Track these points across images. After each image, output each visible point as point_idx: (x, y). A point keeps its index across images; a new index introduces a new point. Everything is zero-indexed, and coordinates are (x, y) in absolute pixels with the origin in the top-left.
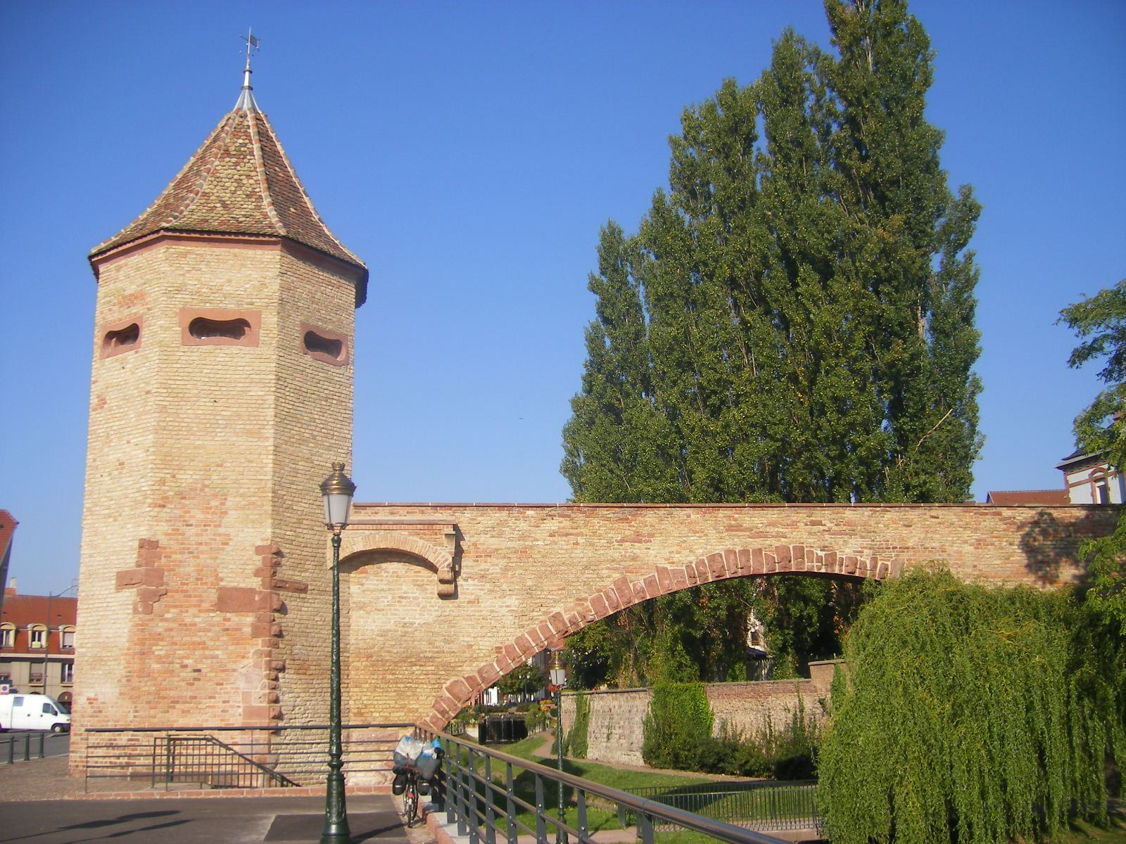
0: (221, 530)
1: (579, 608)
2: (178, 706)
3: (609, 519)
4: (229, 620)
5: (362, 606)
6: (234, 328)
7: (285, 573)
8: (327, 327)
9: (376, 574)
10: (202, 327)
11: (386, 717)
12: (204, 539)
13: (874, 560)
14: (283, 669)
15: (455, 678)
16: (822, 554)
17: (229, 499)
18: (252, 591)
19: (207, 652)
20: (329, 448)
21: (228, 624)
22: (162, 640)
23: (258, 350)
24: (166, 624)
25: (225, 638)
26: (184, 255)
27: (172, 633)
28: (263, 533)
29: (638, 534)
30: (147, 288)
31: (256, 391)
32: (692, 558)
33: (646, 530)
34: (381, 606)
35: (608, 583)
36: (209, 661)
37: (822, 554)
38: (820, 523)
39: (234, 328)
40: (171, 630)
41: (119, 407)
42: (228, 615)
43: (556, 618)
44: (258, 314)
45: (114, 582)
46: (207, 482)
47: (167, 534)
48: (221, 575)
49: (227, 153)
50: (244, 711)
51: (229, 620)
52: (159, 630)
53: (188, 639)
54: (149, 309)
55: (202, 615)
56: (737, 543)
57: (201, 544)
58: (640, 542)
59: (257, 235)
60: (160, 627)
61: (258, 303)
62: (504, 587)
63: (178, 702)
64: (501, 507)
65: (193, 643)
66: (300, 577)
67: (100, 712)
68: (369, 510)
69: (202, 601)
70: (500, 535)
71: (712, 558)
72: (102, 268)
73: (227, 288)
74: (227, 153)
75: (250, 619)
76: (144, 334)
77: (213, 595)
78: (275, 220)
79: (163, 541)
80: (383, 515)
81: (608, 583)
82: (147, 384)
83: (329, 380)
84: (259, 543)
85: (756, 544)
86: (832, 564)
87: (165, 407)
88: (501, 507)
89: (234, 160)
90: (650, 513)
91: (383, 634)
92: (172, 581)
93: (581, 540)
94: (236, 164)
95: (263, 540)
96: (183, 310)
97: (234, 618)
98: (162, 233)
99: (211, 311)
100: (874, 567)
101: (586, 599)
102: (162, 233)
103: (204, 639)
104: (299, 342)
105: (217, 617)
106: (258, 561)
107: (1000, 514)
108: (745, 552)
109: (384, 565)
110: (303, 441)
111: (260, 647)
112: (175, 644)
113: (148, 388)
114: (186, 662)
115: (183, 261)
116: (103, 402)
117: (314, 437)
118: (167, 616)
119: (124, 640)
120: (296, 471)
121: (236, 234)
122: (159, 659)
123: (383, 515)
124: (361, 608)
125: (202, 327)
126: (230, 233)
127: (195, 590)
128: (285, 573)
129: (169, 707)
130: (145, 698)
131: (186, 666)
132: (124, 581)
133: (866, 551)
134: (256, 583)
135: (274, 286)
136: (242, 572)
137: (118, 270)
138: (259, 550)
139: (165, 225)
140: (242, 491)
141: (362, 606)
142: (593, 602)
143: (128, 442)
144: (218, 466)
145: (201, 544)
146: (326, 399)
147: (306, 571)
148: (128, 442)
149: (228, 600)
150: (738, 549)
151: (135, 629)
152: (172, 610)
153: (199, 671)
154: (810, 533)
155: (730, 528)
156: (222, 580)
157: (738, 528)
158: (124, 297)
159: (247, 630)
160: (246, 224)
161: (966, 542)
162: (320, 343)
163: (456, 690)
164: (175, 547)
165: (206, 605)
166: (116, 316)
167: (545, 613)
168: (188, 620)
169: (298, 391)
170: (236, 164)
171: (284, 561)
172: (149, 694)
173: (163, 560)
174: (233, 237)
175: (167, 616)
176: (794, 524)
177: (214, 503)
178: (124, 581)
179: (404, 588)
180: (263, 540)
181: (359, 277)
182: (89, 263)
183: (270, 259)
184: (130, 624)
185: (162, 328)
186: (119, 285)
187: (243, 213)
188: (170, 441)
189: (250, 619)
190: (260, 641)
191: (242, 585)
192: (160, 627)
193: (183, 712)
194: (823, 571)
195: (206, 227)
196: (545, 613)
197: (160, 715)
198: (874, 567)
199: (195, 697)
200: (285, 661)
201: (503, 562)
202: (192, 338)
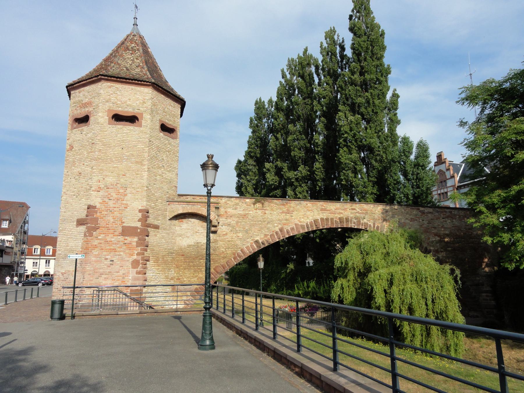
0: (125, 202)
1: (266, 238)
2: (103, 276)
3: (277, 204)
4: (126, 239)
5: (180, 235)
6: (132, 119)
7: (150, 221)
8: (170, 123)
9: (187, 223)
10: (118, 118)
11: (189, 281)
12: (117, 206)
13: (374, 224)
14: (148, 260)
15: (217, 265)
16: (355, 221)
17: (128, 189)
18: (137, 228)
19: (117, 253)
20: (169, 171)
21: (126, 241)
22: (97, 248)
23: (142, 129)
24: (98, 241)
25: (125, 247)
26: (110, 87)
27: (101, 245)
28: (142, 204)
29: (288, 210)
30: (93, 100)
31: (140, 146)
32: (308, 221)
33: (292, 209)
34: (188, 235)
35: (277, 229)
36: (117, 257)
37: (355, 221)
38: (354, 209)
39: (132, 119)
40: (101, 243)
41: (79, 150)
42: (126, 238)
43: (257, 242)
44: (142, 114)
45: (75, 223)
46: (118, 182)
47: (100, 203)
48: (123, 221)
49: (127, 49)
50: (132, 278)
51: (126, 239)
52: (95, 243)
53: (109, 247)
54: (94, 109)
55: (115, 237)
56: (324, 215)
57: (115, 207)
58: (289, 213)
59: (141, 81)
60: (96, 242)
61: (142, 109)
62: (237, 229)
63: (103, 274)
64: (227, 197)
65: (111, 249)
66: (156, 223)
67: (67, 279)
68: (184, 197)
69: (115, 231)
70: (236, 209)
71: (316, 221)
72: (72, 92)
73: (128, 102)
74: (127, 49)
75: (136, 239)
76: (92, 119)
77: (120, 229)
78: (150, 76)
79: (98, 205)
80: (190, 199)
81: (277, 229)
82: (93, 140)
83: (170, 144)
84: (140, 208)
85: (331, 216)
86: (359, 225)
87: (100, 150)
88: (227, 197)
89: (131, 52)
90: (293, 202)
91: (189, 246)
92: (102, 223)
93: (267, 212)
94: (131, 54)
95: (142, 206)
96: (109, 110)
97: (129, 239)
98: (100, 77)
99: (122, 111)
100: (374, 227)
101: (268, 235)
102: (100, 77)
103: (115, 248)
104: (158, 127)
105: (121, 238)
106: (140, 215)
107: (419, 209)
108: (327, 219)
109: (190, 219)
110: (159, 168)
111: (139, 251)
112: (103, 249)
113: (93, 142)
114: (107, 257)
115: (110, 89)
116: (72, 147)
117: (164, 166)
118: (99, 237)
119: (79, 248)
120: (156, 179)
121: (132, 80)
122: (96, 256)
123: (190, 199)
124: (180, 236)
125: (118, 118)
126: (129, 79)
127: (112, 227)
128: (150, 221)
129: (99, 276)
130: (88, 273)
131: (107, 259)
132: (80, 222)
133: (371, 221)
134: (139, 225)
135: (149, 104)
136: (133, 221)
137: (80, 93)
138: (140, 211)
139: (101, 73)
140: (133, 186)
141: (180, 235)
142: (271, 236)
143: (83, 164)
144: (123, 175)
145: (115, 207)
146: (169, 152)
147: (159, 220)
148: (83, 164)
149: (127, 231)
150: (325, 217)
151: (85, 243)
152: (102, 235)
153: (113, 261)
154: (351, 213)
155: (322, 210)
156: (124, 223)
157: (325, 210)
158: (82, 104)
159: (135, 244)
160: (137, 77)
161: (407, 219)
162: (166, 129)
163: (217, 270)
164: (103, 208)
165: (117, 233)
166: (79, 111)
167: (252, 240)
168: (108, 239)
169: (158, 147)
170: (131, 54)
171: (150, 216)
172: (90, 271)
173: (98, 214)
174: (130, 81)
175: (99, 237)
176: (345, 209)
177: (121, 191)
178: (80, 222)
179: (198, 228)
180: (142, 206)
181: (182, 103)
182: (66, 89)
183: (148, 92)
184: (82, 241)
185: (101, 118)
186: (80, 99)
187: (136, 72)
188: (102, 164)
189: (136, 239)
190: (139, 248)
191: (133, 225)
192: (96, 242)
193: (105, 278)
194: (356, 227)
195: (119, 76)
196: (252, 240)
197: (95, 280)
198: (374, 227)
199: (111, 272)
200: (149, 257)
201: (236, 219)
202: (116, 122)
